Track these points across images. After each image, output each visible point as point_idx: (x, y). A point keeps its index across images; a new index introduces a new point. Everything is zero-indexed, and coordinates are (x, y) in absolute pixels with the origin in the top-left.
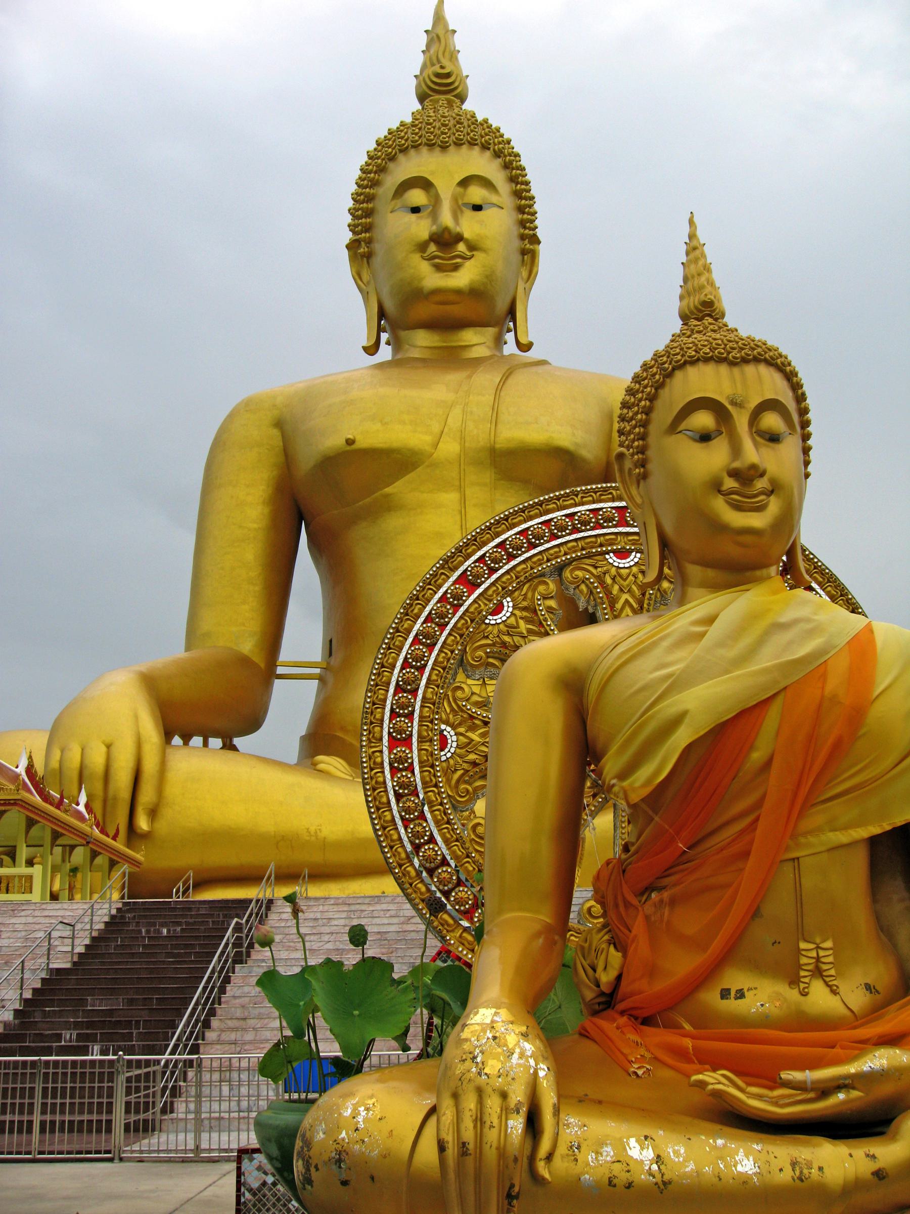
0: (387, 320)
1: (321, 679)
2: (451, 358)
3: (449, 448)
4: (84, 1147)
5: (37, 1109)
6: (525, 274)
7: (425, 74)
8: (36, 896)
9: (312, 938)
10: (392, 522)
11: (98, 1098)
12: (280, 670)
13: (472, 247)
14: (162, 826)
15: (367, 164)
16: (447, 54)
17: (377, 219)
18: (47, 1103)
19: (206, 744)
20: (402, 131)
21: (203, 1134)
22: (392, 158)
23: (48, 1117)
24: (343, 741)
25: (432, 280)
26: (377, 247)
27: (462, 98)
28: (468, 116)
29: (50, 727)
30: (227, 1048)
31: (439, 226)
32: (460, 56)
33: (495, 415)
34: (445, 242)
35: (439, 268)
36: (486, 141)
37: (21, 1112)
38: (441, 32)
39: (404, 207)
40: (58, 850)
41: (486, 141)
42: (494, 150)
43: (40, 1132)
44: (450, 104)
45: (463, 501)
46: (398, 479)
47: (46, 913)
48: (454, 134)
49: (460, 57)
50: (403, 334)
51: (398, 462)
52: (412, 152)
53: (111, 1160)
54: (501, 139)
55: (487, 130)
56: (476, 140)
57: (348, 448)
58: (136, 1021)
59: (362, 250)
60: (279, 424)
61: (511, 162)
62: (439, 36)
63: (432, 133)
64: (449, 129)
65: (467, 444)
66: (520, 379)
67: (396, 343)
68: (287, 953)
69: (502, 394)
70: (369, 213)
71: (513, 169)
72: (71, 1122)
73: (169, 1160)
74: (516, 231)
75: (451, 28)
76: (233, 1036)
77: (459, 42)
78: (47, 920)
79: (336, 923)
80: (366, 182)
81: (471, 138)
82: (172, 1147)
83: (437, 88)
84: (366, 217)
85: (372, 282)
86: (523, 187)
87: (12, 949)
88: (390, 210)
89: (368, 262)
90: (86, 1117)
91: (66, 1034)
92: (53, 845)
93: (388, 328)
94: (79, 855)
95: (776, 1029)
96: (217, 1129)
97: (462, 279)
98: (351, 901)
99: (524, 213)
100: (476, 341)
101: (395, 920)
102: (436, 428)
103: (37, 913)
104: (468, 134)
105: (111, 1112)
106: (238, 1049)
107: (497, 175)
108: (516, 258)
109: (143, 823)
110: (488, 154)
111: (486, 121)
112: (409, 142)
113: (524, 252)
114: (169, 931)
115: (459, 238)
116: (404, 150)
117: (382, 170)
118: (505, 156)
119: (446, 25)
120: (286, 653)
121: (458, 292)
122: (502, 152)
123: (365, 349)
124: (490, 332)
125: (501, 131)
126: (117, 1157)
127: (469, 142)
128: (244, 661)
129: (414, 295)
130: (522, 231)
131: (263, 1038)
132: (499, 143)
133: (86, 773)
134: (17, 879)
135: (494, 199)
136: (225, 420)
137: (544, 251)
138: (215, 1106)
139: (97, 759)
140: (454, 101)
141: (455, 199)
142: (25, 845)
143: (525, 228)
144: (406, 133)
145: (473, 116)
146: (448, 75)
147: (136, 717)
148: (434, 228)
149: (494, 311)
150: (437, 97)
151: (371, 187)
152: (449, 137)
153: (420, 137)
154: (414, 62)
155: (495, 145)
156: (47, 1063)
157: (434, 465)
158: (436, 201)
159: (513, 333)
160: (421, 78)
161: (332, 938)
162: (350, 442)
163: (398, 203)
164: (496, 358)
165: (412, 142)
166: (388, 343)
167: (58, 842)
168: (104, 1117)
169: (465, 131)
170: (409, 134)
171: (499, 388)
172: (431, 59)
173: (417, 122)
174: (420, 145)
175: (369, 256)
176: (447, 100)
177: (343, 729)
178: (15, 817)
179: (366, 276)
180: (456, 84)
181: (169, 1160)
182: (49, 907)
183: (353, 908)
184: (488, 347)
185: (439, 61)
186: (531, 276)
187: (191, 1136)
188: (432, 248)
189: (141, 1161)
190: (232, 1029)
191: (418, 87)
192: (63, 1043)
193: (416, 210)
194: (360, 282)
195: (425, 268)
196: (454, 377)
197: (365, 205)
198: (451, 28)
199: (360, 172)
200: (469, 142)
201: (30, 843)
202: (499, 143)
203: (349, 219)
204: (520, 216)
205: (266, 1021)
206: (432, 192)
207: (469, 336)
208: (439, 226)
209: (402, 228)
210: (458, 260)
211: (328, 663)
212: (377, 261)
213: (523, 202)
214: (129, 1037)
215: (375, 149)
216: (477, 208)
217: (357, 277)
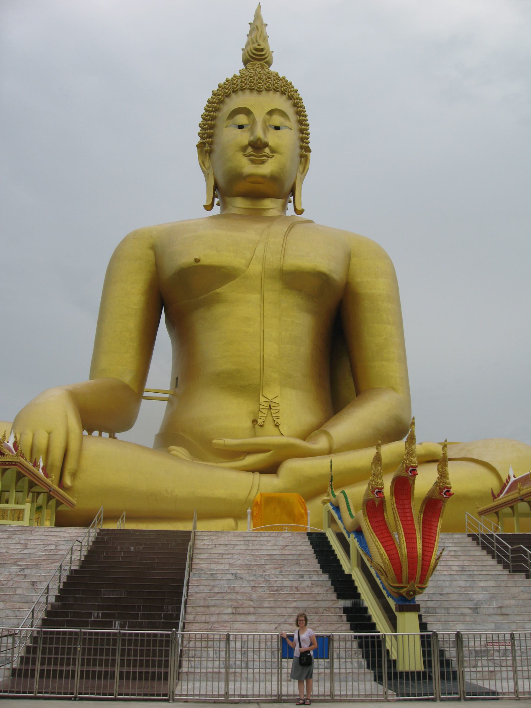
1: (169, 400)
2: (256, 215)
3: (256, 268)
4: (149, 691)
5: (78, 662)
6: (301, 169)
7: (248, 48)
8: (26, 522)
9: (227, 556)
10: (220, 310)
11: (67, 655)
12: (145, 394)
13: (273, 151)
14: (79, 484)
15: (213, 98)
16: (262, 38)
18: (84, 659)
19: (100, 435)
20: (234, 80)
21: (230, 683)
22: (228, 96)
23: (46, 667)
25: (248, 168)
26: (216, 147)
27: (269, 64)
28: (274, 75)
29: (13, 421)
30: (202, 626)
31: (251, 137)
32: (269, 39)
33: (283, 250)
34: (257, 147)
35: (253, 162)
36: (284, 90)
37: (107, 665)
38: (259, 25)
39: (234, 124)
40: (31, 494)
41: (284, 90)
42: (288, 95)
43: (40, 677)
44: (262, 67)
46: (224, 284)
47: (52, 534)
48: (266, 84)
49: (269, 40)
50: (228, 199)
51: (223, 275)
52: (240, 93)
53: (167, 700)
54: (292, 89)
55: (285, 83)
56: (278, 88)
57: (196, 264)
58: (138, 606)
59: (206, 148)
60: (153, 247)
61: (298, 103)
62: (257, 27)
63: (252, 82)
64: (263, 81)
65: (266, 266)
66: (298, 230)
67: (224, 205)
68: (215, 565)
69: (288, 238)
70: (212, 127)
71: (298, 107)
72: (140, 673)
73: (205, 702)
74: (298, 143)
75: (264, 23)
76: (203, 618)
77: (268, 31)
78: (54, 538)
79: (239, 547)
80: (211, 109)
81: (276, 87)
82: (203, 692)
83: (258, 57)
84: (210, 129)
85: (211, 168)
86: (304, 118)
87: (37, 556)
88: (225, 125)
90: (97, 669)
91: (95, 613)
92: (29, 491)
93: (219, 195)
94: (41, 499)
96: (218, 679)
97: (268, 168)
98: (244, 534)
99: (303, 133)
100: (271, 205)
101: (276, 547)
102: (248, 256)
103: (46, 534)
104: (274, 85)
105: (168, 667)
106: (210, 627)
108: (298, 159)
109: (68, 481)
110: (285, 97)
111: (284, 78)
112: (239, 87)
113: (301, 156)
114: (135, 548)
115: (266, 145)
116: (235, 91)
117: (221, 102)
118: (294, 99)
119: (262, 21)
120: (149, 384)
121: (264, 177)
122: (293, 97)
123: (205, 207)
124: (280, 201)
125: (293, 84)
126: (171, 699)
127: (274, 89)
128: (126, 387)
129: (236, 177)
130: (301, 144)
131: (223, 620)
132: (292, 91)
133: (35, 449)
134: (9, 512)
135: (287, 123)
137: (313, 157)
138: (210, 664)
139: (42, 441)
140: (265, 66)
141: (265, 122)
142: (15, 491)
143: (303, 142)
144: (237, 81)
145: (277, 74)
146: (262, 50)
147: (66, 416)
148: (252, 138)
149: (282, 189)
150: (255, 62)
151: (214, 112)
152: (263, 86)
153: (245, 84)
155: (289, 92)
156: (85, 633)
158: (254, 122)
159: (292, 203)
160: (246, 51)
161: (240, 557)
162: (197, 261)
163: (230, 122)
164: (282, 217)
165: (241, 87)
166: (218, 204)
167: (33, 490)
168: (163, 670)
169: (272, 83)
170: (239, 82)
171: (287, 234)
172: (252, 40)
173: (244, 76)
174: (245, 89)
175: (210, 152)
176: (261, 64)
178: (11, 474)
179: (207, 164)
180: (266, 56)
181: (205, 702)
182: (53, 530)
183: (246, 539)
184: (278, 210)
185: (257, 41)
187: (222, 685)
188: (250, 150)
189: (186, 701)
190: (203, 613)
192: (93, 619)
193: (241, 127)
194: (204, 168)
196: (259, 227)
198: (264, 23)
199: (207, 103)
200: (274, 89)
201: (17, 490)
202: (292, 91)
203: (198, 130)
204: (301, 135)
205: (222, 609)
207: (268, 203)
208: (251, 137)
209: (232, 137)
210: (265, 158)
212: (215, 156)
213: (303, 127)
214: (136, 616)
215: (218, 90)
216: (277, 128)
217: (202, 164)
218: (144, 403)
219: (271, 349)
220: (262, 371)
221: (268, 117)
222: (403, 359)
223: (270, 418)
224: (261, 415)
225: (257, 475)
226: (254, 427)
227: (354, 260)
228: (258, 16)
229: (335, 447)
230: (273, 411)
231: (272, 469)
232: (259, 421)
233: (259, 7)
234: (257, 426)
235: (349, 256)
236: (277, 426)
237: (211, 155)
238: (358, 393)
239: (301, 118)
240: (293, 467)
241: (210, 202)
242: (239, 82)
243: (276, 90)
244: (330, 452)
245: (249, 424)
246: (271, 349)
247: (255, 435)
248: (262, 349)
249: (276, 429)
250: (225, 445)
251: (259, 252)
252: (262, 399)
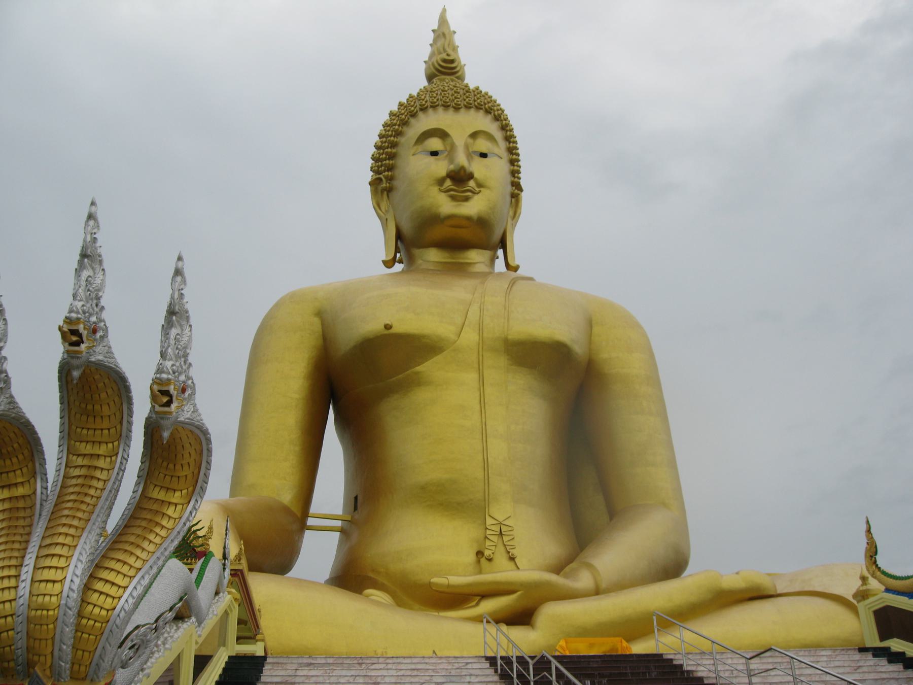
0: (402, 241)
1: (342, 531)
2: (460, 269)
6: (511, 213)
7: (434, 59)
10: (421, 395)
12: (311, 522)
13: (480, 185)
17: (399, 162)
22: (414, 115)
25: (446, 206)
34: (459, 179)
35: (453, 198)
39: (424, 151)
50: (416, 252)
57: (387, 332)
60: (320, 314)
65: (485, 335)
67: (410, 261)
70: (392, 156)
74: (509, 179)
77: (458, 40)
84: (389, 159)
85: (391, 211)
88: (412, 152)
89: (388, 196)
97: (473, 207)
100: (475, 256)
107: (498, 135)
108: (508, 198)
110: (490, 117)
115: (471, 176)
116: (423, 109)
117: (405, 123)
121: (468, 218)
123: (384, 262)
124: (487, 254)
128: (286, 510)
136: (271, 309)
137: (525, 197)
141: (467, 147)
146: (452, 61)
148: (452, 167)
149: (485, 237)
150: (443, 77)
158: (453, 147)
162: (388, 327)
163: (419, 148)
170: (428, 98)
175: (389, 190)
177: (373, 571)
179: (384, 205)
185: (445, 50)
186: (515, 215)
188: (448, 183)
193: (434, 154)
197: (389, 150)
206: (448, 141)
209: (421, 168)
211: (352, 517)
212: (396, 196)
216: (483, 155)
221: (470, 141)
222: (672, 464)
223: (501, 549)
224: (488, 543)
226: (479, 562)
227: (596, 330)
228: (443, 21)
230: (505, 538)
231: (522, 617)
232: (487, 553)
233: (444, 10)
234: (483, 560)
236: (512, 559)
237: (390, 194)
239: (511, 145)
240: (552, 614)
241: (391, 256)
242: (428, 98)
243: (478, 108)
244: (597, 592)
245: (472, 557)
248: (485, 450)
250: (449, 586)
252: (489, 521)
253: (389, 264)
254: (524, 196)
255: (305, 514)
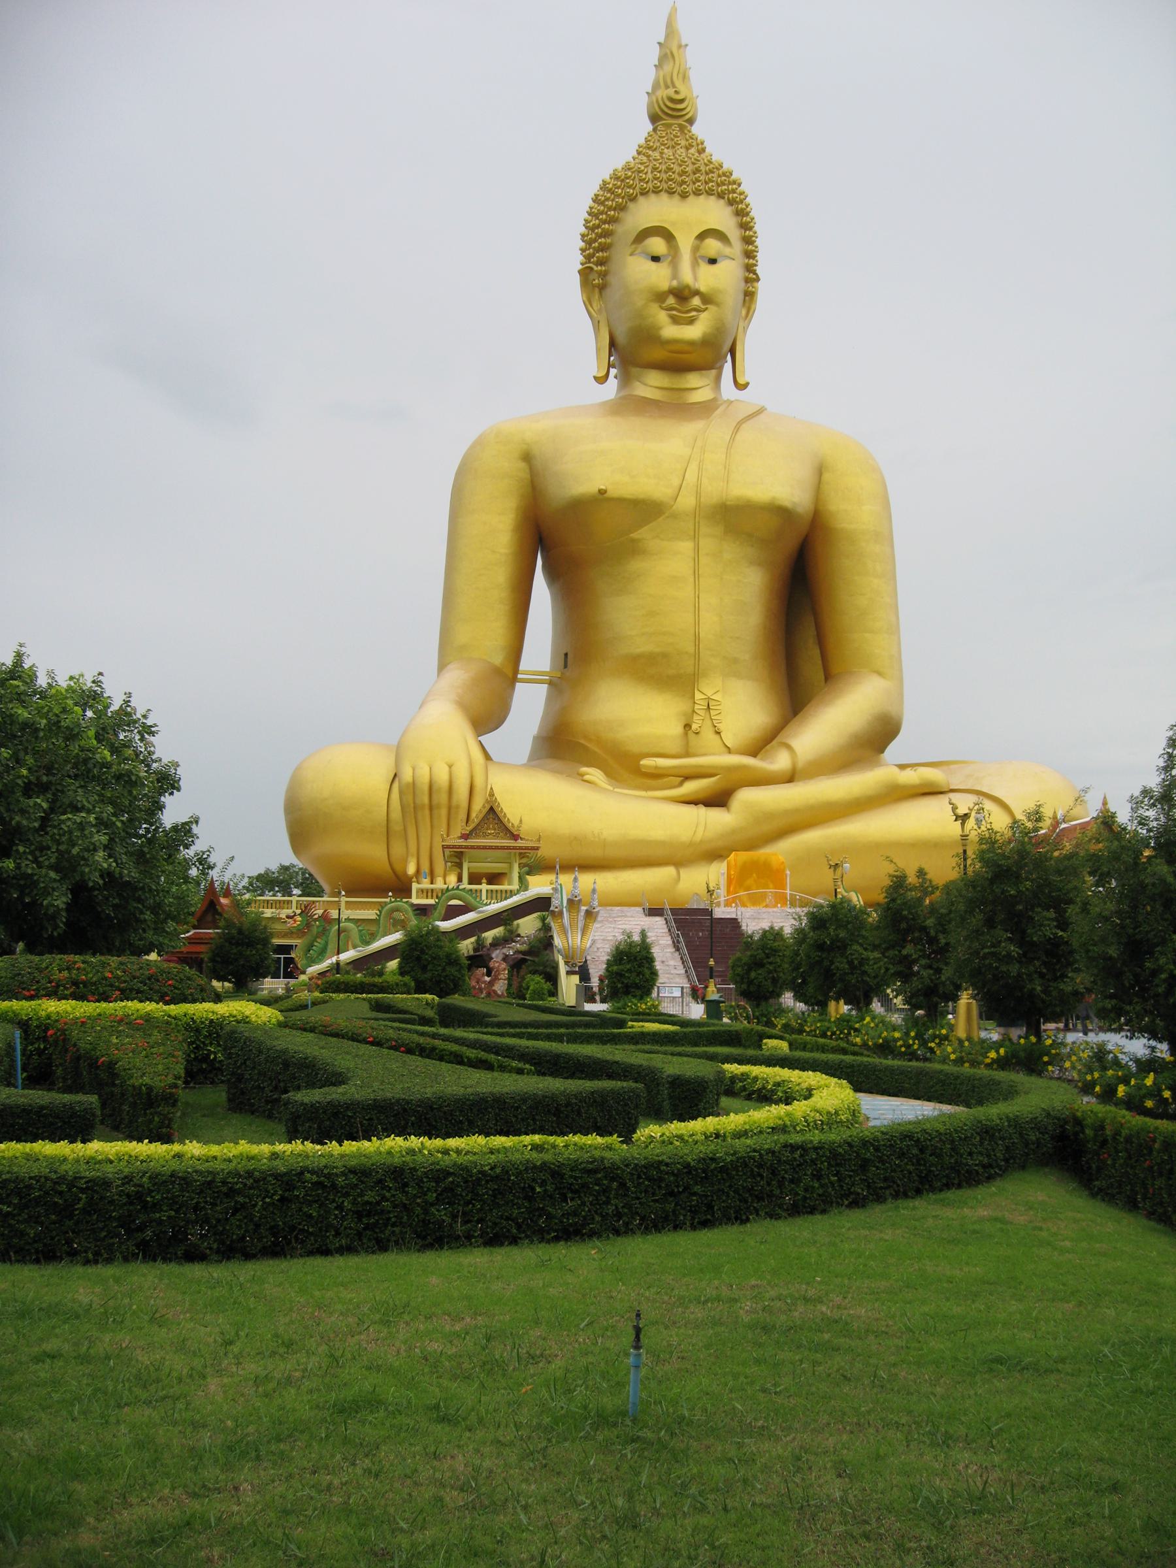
1: (550, 683)
3: (686, 501)
6: (744, 312)
10: (636, 565)
24: (586, 749)
25: (671, 331)
26: (611, 279)
35: (675, 321)
45: (697, 549)
50: (635, 371)
57: (601, 497)
60: (527, 457)
66: (747, 433)
67: (626, 379)
83: (670, 112)
95: (563, 1014)
97: (693, 332)
100: (698, 387)
107: (734, 234)
110: (722, 202)
121: (691, 343)
133: (435, 788)
139: (442, 776)
141: (695, 249)
146: (682, 101)
148: (675, 283)
154: (648, 77)
157: (674, 516)
175: (602, 288)
177: (586, 737)
188: (671, 301)
191: (650, 106)
193: (656, 259)
195: (662, 317)
196: (690, 428)
207: (693, 380)
209: (640, 273)
210: (694, 313)
212: (607, 292)
216: (713, 261)
218: (519, 686)
219: (709, 623)
220: (697, 656)
221: (698, 242)
223: (709, 723)
225: (702, 810)
227: (826, 476)
228: (671, 30)
229: (800, 764)
231: (718, 800)
232: (694, 726)
235: (820, 470)
236: (718, 733)
238: (828, 676)
240: (746, 797)
244: (790, 778)
245: (678, 729)
246: (709, 623)
247: (687, 754)
248: (697, 623)
249: (717, 737)
250: (656, 767)
251: (691, 477)
252: (698, 696)
253: (602, 380)
254: (761, 287)
255: (516, 670)
